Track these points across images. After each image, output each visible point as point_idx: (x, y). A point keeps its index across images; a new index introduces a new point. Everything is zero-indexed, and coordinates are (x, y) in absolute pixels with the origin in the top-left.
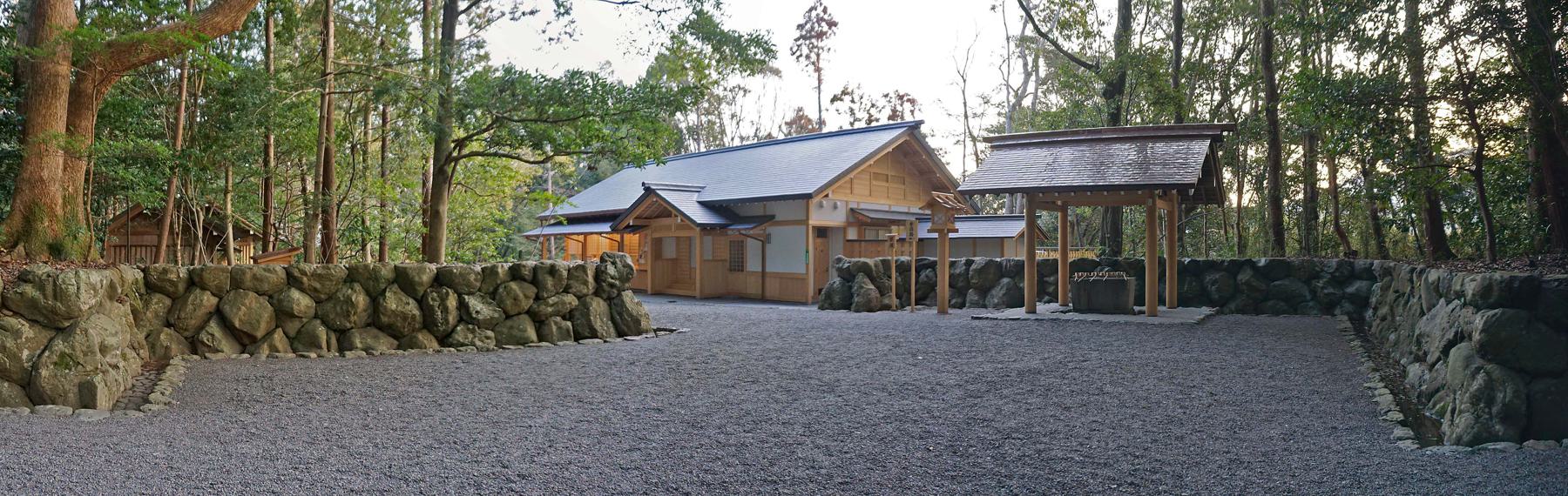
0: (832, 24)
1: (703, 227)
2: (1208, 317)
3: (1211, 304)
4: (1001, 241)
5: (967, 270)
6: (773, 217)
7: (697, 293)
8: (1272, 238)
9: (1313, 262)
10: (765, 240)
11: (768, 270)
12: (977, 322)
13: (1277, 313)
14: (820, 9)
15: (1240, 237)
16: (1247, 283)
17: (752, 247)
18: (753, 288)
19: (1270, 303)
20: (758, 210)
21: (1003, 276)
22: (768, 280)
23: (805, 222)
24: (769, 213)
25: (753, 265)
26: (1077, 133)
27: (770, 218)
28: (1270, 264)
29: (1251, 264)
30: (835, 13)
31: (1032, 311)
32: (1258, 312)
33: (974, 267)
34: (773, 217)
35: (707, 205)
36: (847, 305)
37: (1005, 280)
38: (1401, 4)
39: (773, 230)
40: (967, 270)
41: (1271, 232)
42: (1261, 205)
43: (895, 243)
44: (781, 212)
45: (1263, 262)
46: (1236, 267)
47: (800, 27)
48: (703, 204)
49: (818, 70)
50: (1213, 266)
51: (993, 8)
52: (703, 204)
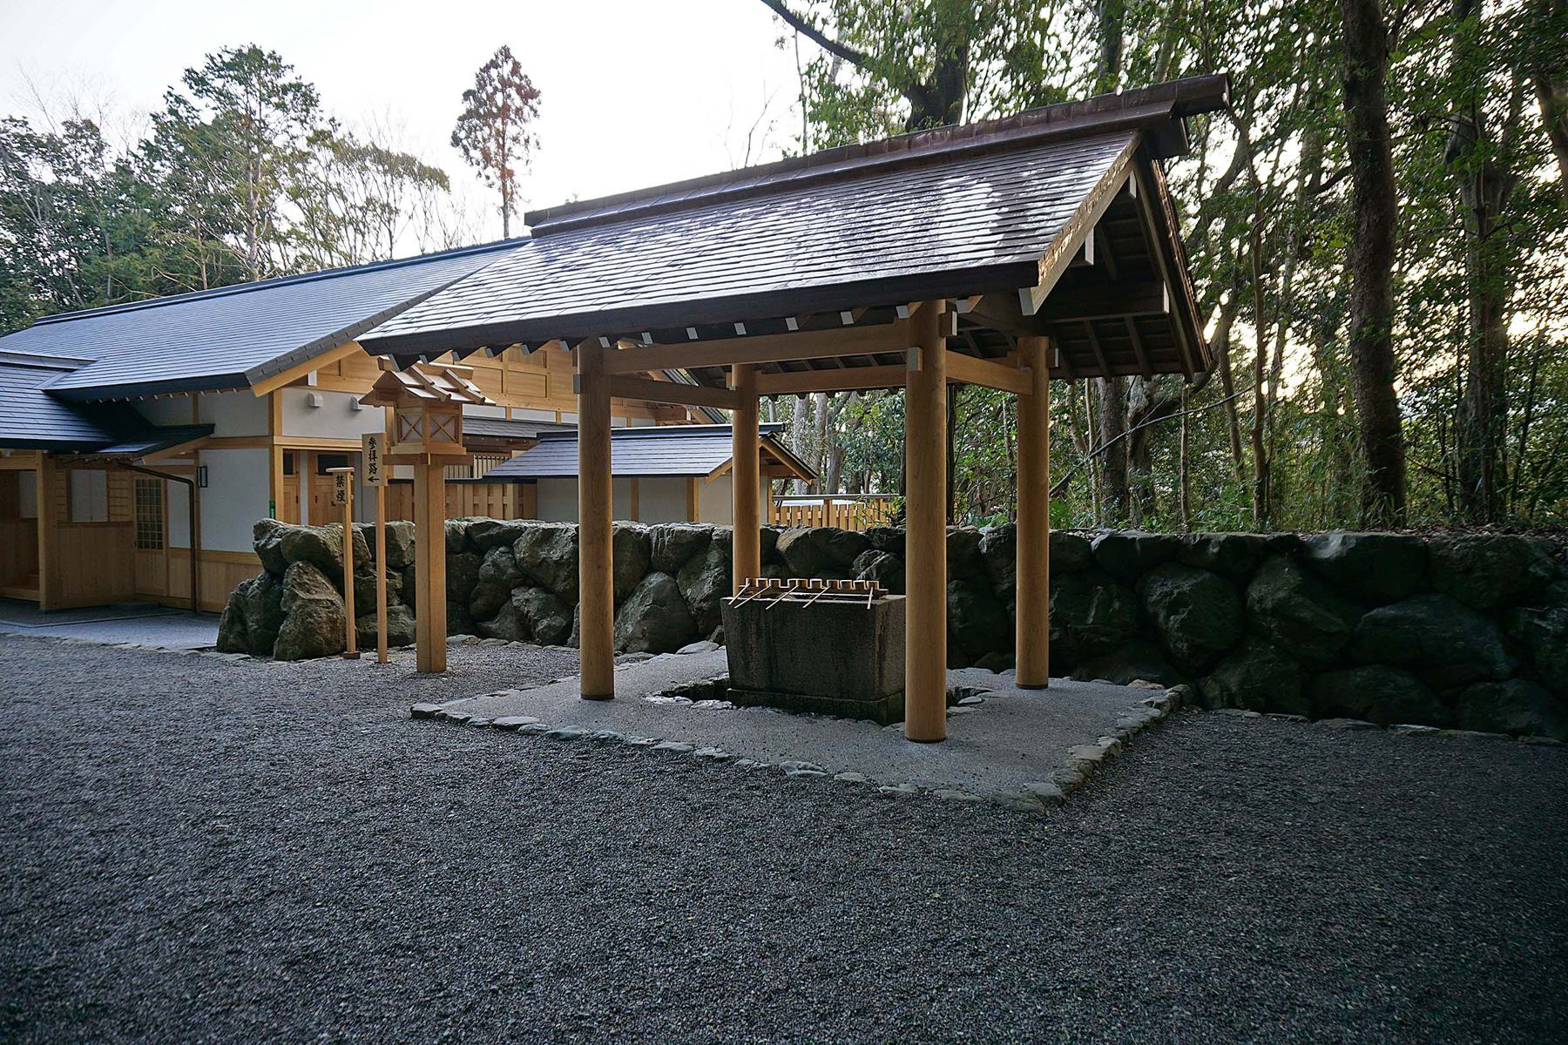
0: (529, 94)
1: (54, 450)
2: (1132, 740)
3: (1164, 667)
4: (689, 480)
7: (41, 595)
8: (1361, 469)
9: (1520, 550)
10: (198, 482)
11: (207, 544)
12: (424, 730)
13: (1383, 714)
14: (507, 69)
15: (1264, 468)
16: (1279, 610)
19: (1360, 676)
20: (180, 413)
21: (650, 570)
22: (205, 568)
23: (266, 440)
25: (178, 537)
28: (1360, 555)
29: (1296, 551)
31: (600, 692)
32: (1319, 710)
36: (262, 647)
37: (655, 579)
39: (210, 457)
41: (1359, 457)
42: (1328, 392)
43: (508, 495)
44: (225, 415)
45: (1334, 544)
46: (1244, 560)
47: (467, 95)
48: (56, 397)
49: (506, 174)
50: (1170, 555)
51: (782, 40)
52: (56, 397)
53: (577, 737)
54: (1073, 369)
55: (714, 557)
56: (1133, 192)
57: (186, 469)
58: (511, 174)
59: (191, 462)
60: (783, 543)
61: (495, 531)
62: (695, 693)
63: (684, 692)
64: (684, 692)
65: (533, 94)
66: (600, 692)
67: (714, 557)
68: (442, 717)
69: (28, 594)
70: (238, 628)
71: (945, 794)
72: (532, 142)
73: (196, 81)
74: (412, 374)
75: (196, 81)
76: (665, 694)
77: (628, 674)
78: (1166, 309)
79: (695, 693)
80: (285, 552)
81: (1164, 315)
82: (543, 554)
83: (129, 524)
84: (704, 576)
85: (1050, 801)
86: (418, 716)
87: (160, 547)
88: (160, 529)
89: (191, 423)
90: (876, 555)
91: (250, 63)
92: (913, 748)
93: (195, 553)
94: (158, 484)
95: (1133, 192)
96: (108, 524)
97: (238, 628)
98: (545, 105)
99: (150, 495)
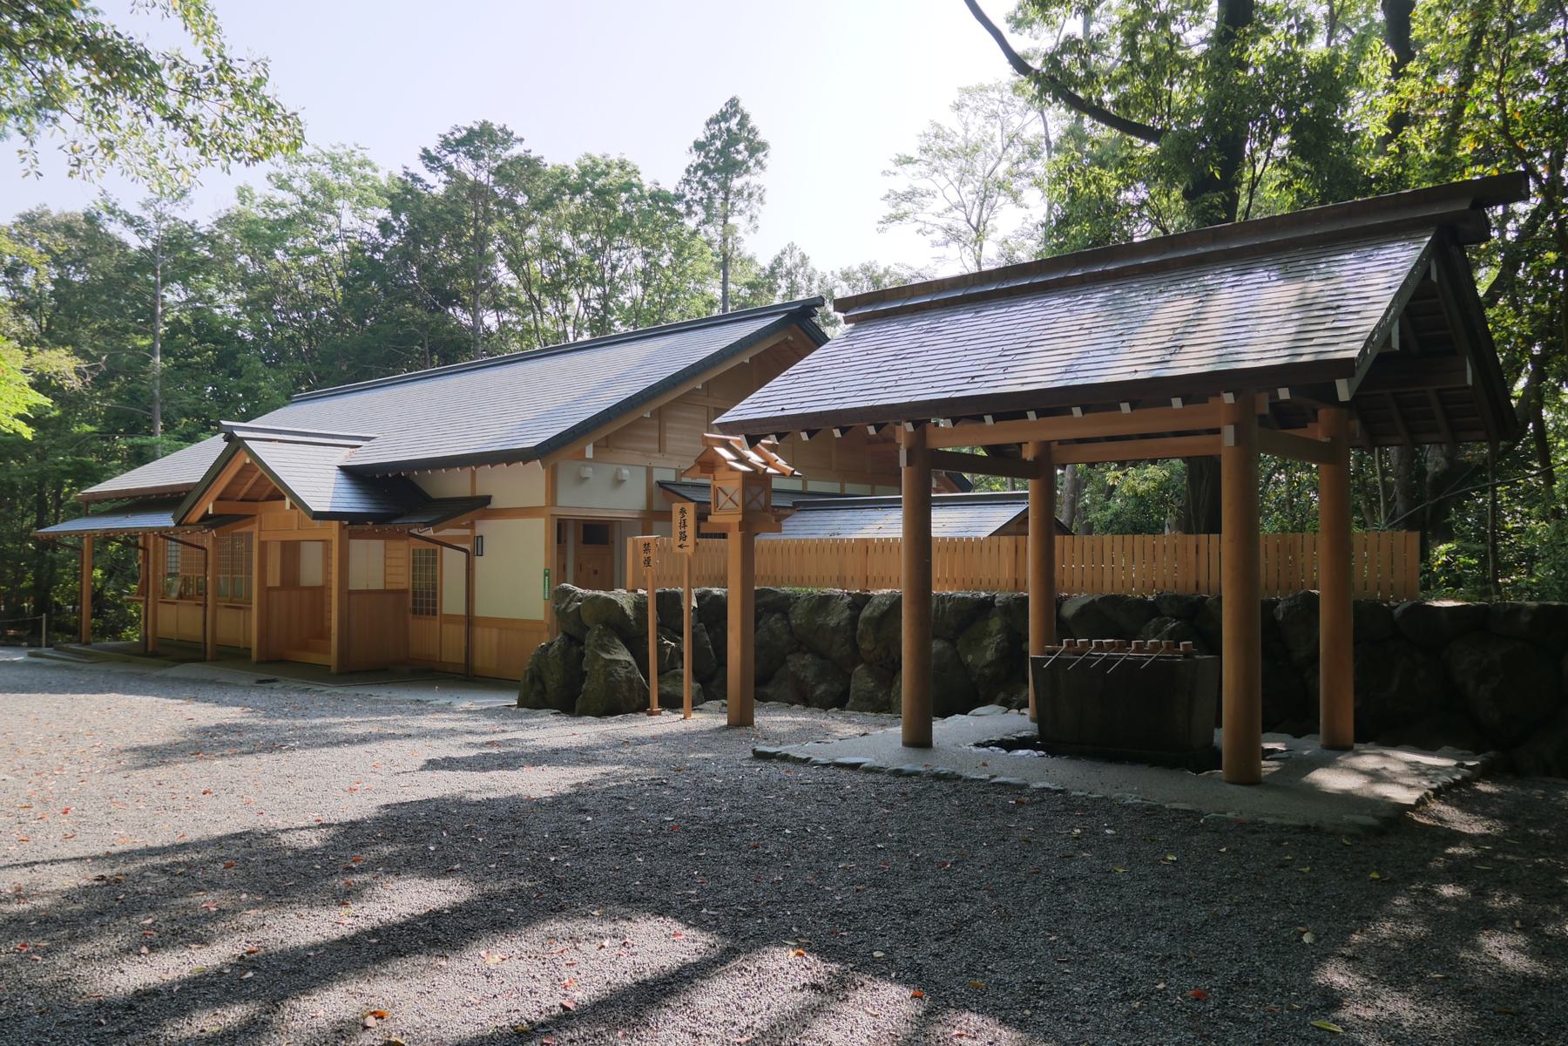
0: (756, 148)
5: (854, 620)
6: (488, 499)
7: (332, 659)
10: (475, 549)
17: (452, 562)
18: (451, 643)
20: (457, 485)
24: (480, 492)
26: (307, 434)
27: (479, 505)
30: (763, 125)
31: (919, 739)
33: (866, 612)
34: (488, 499)
35: (355, 475)
38: (1378, 6)
39: (485, 527)
40: (854, 620)
44: (504, 487)
47: (699, 146)
48: (349, 472)
52: (349, 472)
53: (917, 774)
54: (1374, 439)
55: (995, 624)
56: (1434, 277)
57: (465, 539)
58: (733, 229)
59: (467, 532)
60: (1069, 610)
61: (770, 598)
62: (1009, 745)
63: (1001, 744)
64: (1001, 744)
65: (763, 146)
66: (919, 739)
67: (995, 624)
68: (785, 758)
69: (314, 658)
70: (539, 687)
71: (1270, 821)
72: (756, 197)
73: (428, 158)
74: (758, 452)
75: (428, 158)
76: (977, 745)
77: (945, 729)
78: (1470, 382)
79: (1009, 745)
80: (585, 616)
81: (1467, 387)
82: (820, 621)
83: (405, 591)
84: (986, 643)
85: (1368, 829)
86: (760, 756)
87: (434, 613)
88: (435, 595)
89: (468, 494)
90: (1166, 622)
91: (478, 139)
92: (1232, 788)
93: (470, 620)
94: (435, 552)
95: (1434, 277)
96: (385, 592)
97: (539, 687)
98: (772, 159)
99: (426, 563)
